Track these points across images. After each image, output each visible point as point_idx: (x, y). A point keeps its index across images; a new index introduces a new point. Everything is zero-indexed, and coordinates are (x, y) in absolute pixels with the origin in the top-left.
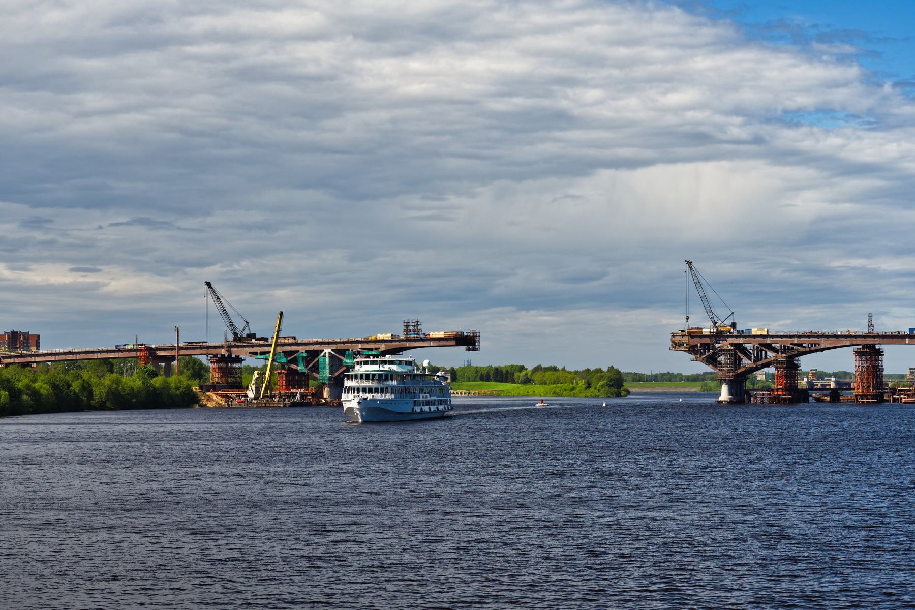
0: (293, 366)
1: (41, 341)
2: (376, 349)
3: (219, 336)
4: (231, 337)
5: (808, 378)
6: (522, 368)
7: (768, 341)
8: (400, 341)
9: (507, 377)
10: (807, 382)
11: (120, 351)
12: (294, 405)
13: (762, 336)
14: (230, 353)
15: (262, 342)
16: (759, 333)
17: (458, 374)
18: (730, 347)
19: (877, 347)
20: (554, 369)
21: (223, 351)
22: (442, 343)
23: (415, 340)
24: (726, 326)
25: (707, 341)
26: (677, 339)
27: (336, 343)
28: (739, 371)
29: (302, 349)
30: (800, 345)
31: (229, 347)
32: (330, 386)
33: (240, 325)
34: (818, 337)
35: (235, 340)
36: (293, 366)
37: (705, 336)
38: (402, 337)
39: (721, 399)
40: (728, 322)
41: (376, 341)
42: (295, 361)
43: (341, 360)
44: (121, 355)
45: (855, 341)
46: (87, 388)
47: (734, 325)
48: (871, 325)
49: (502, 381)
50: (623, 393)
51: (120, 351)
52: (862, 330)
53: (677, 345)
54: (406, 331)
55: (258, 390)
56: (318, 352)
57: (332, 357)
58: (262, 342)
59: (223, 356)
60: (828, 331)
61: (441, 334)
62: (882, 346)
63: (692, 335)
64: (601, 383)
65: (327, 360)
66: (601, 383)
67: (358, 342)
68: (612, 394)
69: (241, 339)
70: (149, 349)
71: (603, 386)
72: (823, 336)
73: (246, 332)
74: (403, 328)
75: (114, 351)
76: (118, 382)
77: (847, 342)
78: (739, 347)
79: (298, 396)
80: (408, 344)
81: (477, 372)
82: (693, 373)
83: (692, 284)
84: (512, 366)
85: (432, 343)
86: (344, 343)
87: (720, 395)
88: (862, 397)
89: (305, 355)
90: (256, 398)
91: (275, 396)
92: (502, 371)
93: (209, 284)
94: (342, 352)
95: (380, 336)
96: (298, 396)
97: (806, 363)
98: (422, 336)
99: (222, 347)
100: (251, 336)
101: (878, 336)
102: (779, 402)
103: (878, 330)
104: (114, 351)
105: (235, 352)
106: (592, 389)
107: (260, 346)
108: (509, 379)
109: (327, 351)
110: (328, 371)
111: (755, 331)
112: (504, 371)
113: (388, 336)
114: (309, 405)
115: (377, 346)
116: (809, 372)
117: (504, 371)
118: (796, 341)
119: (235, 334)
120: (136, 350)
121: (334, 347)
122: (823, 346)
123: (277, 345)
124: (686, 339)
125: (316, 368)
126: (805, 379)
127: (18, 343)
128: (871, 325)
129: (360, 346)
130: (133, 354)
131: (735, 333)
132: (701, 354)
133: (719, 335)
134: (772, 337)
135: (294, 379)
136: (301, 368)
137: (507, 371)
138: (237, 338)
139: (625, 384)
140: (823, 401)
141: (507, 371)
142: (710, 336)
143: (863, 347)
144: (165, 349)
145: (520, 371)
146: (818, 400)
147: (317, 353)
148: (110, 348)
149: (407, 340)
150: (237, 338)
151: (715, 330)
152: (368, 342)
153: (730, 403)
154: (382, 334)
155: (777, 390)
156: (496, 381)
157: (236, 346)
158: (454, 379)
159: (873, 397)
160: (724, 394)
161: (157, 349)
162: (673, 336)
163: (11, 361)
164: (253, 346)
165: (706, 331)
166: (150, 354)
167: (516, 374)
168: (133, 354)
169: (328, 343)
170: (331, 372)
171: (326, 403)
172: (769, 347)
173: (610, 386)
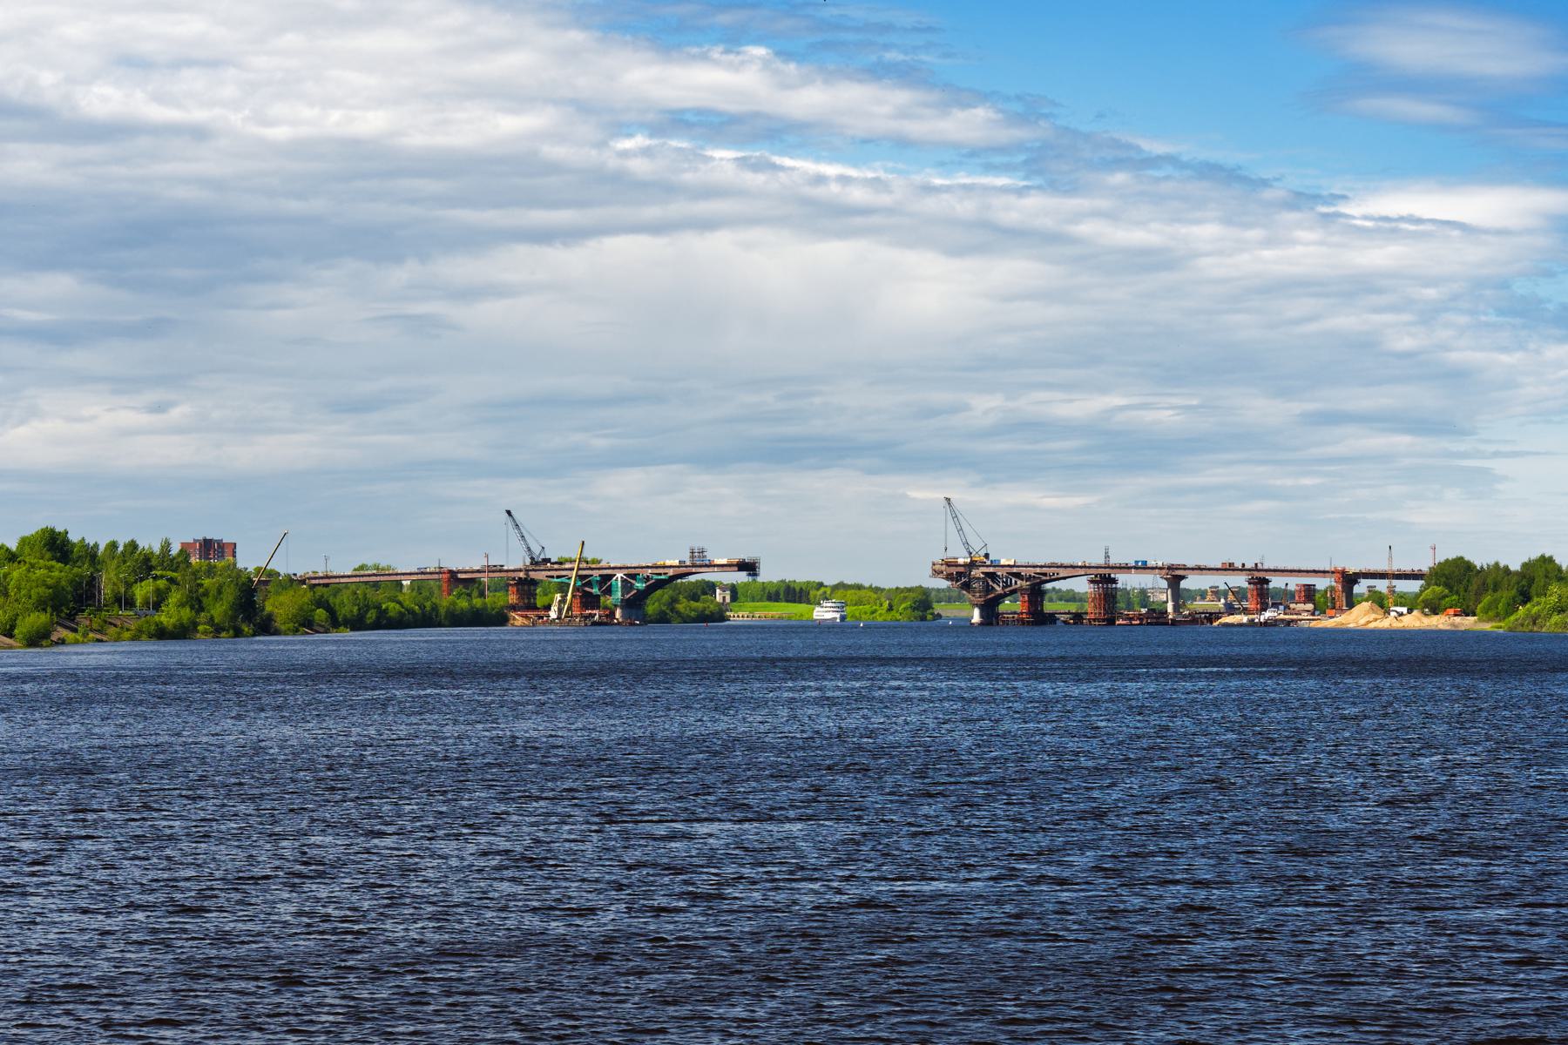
0: (587, 589)
1: (237, 550)
2: (665, 574)
3: (515, 560)
4: (528, 561)
5: (1226, 599)
6: (821, 585)
7: (1015, 570)
8: (686, 567)
9: (800, 597)
10: (1225, 604)
11: (422, 573)
12: (595, 624)
13: (1009, 566)
14: (527, 575)
15: (556, 566)
16: (1007, 563)
17: (740, 591)
18: (982, 576)
19: (1112, 576)
20: (859, 587)
21: (522, 575)
22: (725, 569)
23: (701, 566)
24: (980, 558)
25: (961, 569)
26: (937, 567)
27: (627, 568)
28: (990, 596)
29: (596, 573)
30: (1045, 574)
31: (527, 571)
32: (622, 607)
33: (536, 550)
34: (1058, 567)
35: (532, 564)
36: (587, 589)
37: (960, 566)
38: (688, 563)
39: (973, 621)
40: (982, 553)
41: (664, 567)
42: (589, 584)
43: (632, 584)
44: (423, 577)
45: (1089, 571)
46: (435, 608)
47: (987, 556)
48: (1107, 557)
49: (795, 602)
50: (929, 617)
51: (422, 573)
52: (1101, 562)
53: (936, 573)
54: (692, 557)
55: (560, 611)
56: (610, 577)
57: (623, 581)
58: (556, 566)
59: (520, 578)
60: (1066, 562)
61: (724, 561)
62: (1117, 576)
63: (948, 564)
64: (903, 606)
65: (619, 584)
66: (903, 606)
67: (648, 567)
68: (915, 618)
69: (537, 563)
70: (450, 572)
71: (905, 609)
72: (1061, 566)
73: (542, 556)
74: (689, 554)
75: (417, 574)
76: (454, 603)
77: (1082, 572)
78: (993, 576)
79: (597, 617)
80: (694, 570)
81: (764, 589)
82: (1368, 568)
83: (950, 517)
84: (808, 582)
85: (716, 569)
86: (635, 568)
87: (972, 617)
88: (1094, 620)
89: (598, 579)
90: (559, 618)
91: (576, 617)
92: (794, 589)
93: (509, 513)
94: (633, 576)
95: (668, 563)
96: (597, 617)
97: (1191, 583)
98: (707, 563)
99: (520, 570)
100: (547, 561)
101: (1113, 568)
102: (1023, 624)
103: (1113, 561)
104: (417, 574)
105: (533, 575)
106: (893, 613)
107: (556, 570)
108: (804, 598)
109: (619, 575)
110: (620, 594)
111: (1003, 562)
112: (798, 589)
113: (676, 563)
114: (605, 624)
115: (666, 570)
116: (1206, 591)
117: (798, 589)
118: (1038, 570)
119: (532, 559)
120: (440, 573)
121: (626, 571)
122: (1061, 575)
123: (579, 569)
124: (944, 567)
125: (609, 591)
126: (1223, 601)
127: (211, 552)
128: (1107, 557)
129: (650, 571)
130: (436, 576)
131: (988, 563)
132: (957, 581)
133: (972, 565)
134: (1018, 566)
135: (589, 601)
136: (595, 591)
137: (801, 589)
138: (534, 562)
139: (935, 605)
140: (1069, 623)
141: (801, 589)
142: (965, 565)
143: (1096, 576)
144: (466, 572)
145: (818, 589)
146: (1065, 622)
147: (610, 577)
148: (413, 571)
149: (694, 566)
150: (534, 562)
151: (969, 560)
152: (657, 567)
153: (981, 624)
154: (670, 559)
155: (1022, 613)
156: (787, 601)
157: (533, 570)
158: (734, 598)
159: (1104, 620)
160: (976, 617)
161: (459, 572)
162: (934, 564)
163: (317, 582)
164: (549, 570)
165: (961, 561)
166: (452, 577)
167: (812, 593)
168: (436, 576)
169: (620, 568)
170: (623, 595)
171: (619, 623)
172: (1018, 575)
173: (914, 609)
